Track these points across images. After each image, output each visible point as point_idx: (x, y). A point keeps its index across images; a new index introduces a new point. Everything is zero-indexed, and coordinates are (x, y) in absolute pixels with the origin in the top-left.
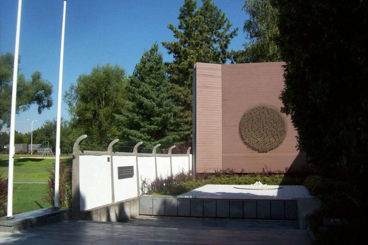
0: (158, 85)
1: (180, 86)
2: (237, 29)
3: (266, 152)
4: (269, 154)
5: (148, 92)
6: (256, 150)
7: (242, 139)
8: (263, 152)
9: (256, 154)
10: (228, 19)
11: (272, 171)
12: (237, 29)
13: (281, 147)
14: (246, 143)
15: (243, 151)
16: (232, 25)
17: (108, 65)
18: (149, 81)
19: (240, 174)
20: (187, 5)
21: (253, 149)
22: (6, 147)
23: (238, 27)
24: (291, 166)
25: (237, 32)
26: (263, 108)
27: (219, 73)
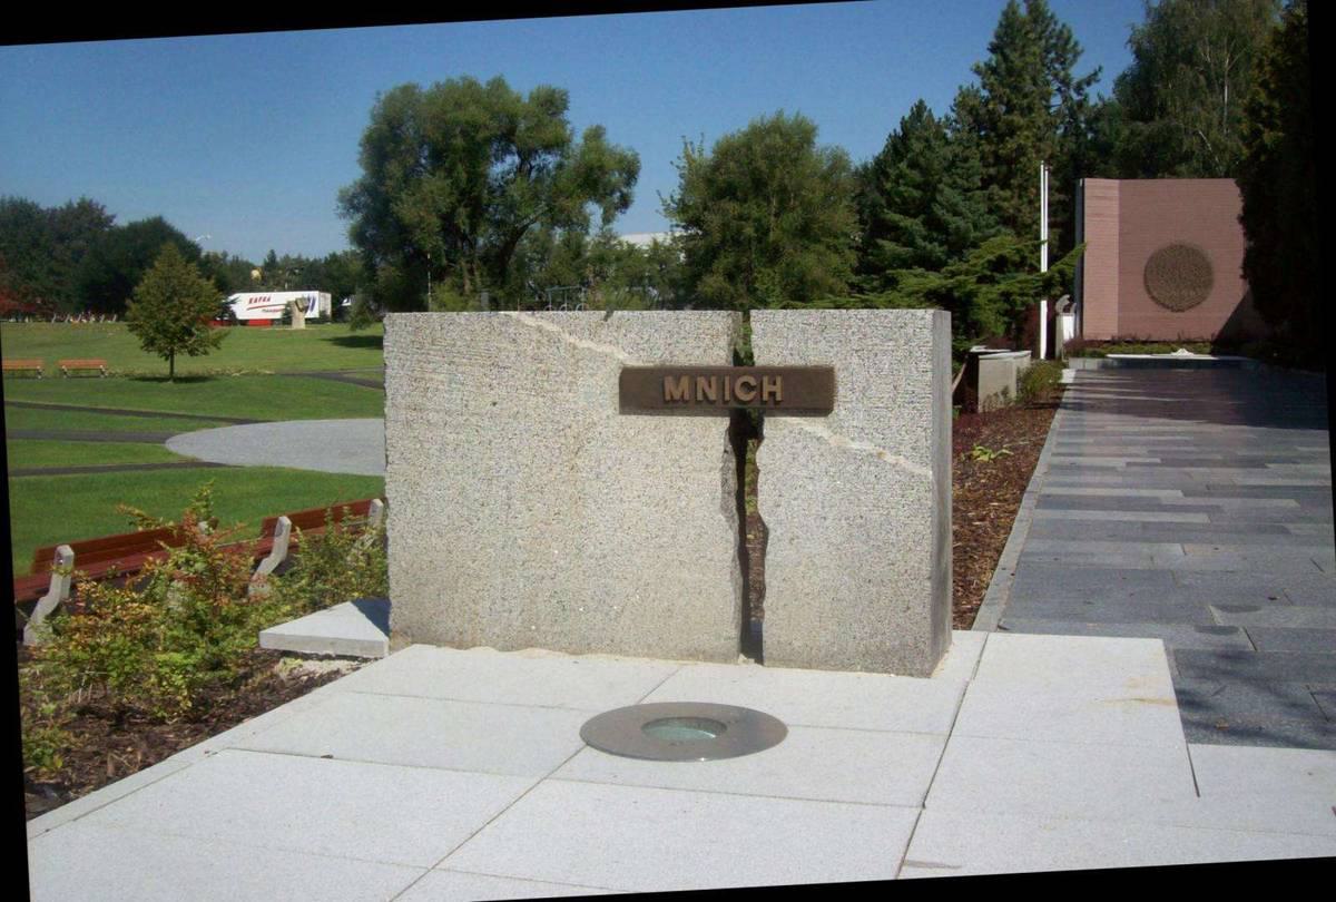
0: (968, 190)
1: (1002, 189)
2: (1100, 69)
3: (1182, 311)
4: (1188, 314)
5: (956, 205)
6: (1168, 308)
7: (1149, 292)
8: (1178, 311)
9: (1168, 313)
10: (1068, 25)
11: (1193, 337)
12: (1100, 69)
13: (1204, 304)
14: (1153, 298)
15: (1152, 310)
16: (1082, 51)
17: (780, 113)
18: (950, 181)
19: (1144, 343)
20: (1009, 37)
21: (1164, 305)
22: (349, 304)
23: (1102, 65)
24: (1222, 332)
25: (1100, 75)
26: (1181, 247)
27: (1116, 193)
